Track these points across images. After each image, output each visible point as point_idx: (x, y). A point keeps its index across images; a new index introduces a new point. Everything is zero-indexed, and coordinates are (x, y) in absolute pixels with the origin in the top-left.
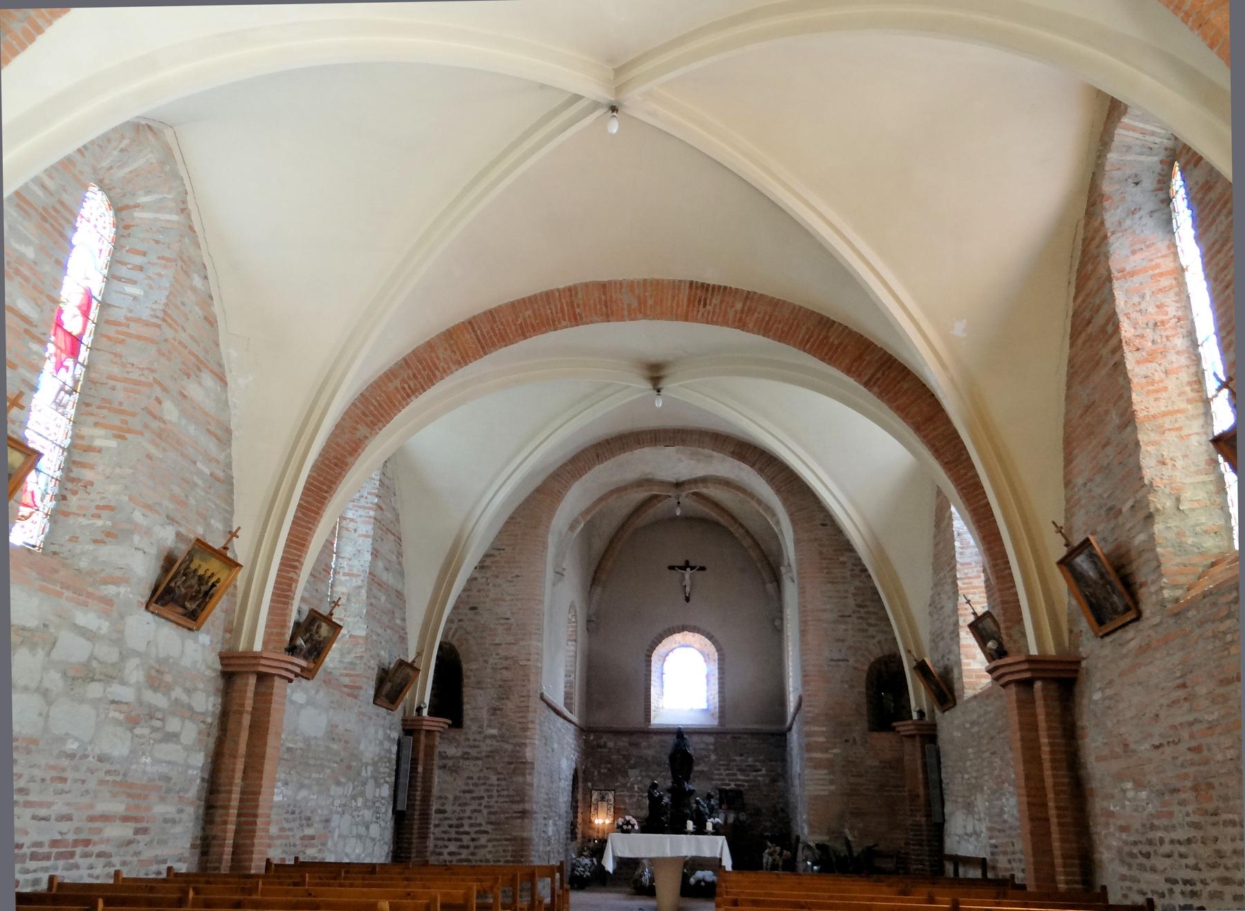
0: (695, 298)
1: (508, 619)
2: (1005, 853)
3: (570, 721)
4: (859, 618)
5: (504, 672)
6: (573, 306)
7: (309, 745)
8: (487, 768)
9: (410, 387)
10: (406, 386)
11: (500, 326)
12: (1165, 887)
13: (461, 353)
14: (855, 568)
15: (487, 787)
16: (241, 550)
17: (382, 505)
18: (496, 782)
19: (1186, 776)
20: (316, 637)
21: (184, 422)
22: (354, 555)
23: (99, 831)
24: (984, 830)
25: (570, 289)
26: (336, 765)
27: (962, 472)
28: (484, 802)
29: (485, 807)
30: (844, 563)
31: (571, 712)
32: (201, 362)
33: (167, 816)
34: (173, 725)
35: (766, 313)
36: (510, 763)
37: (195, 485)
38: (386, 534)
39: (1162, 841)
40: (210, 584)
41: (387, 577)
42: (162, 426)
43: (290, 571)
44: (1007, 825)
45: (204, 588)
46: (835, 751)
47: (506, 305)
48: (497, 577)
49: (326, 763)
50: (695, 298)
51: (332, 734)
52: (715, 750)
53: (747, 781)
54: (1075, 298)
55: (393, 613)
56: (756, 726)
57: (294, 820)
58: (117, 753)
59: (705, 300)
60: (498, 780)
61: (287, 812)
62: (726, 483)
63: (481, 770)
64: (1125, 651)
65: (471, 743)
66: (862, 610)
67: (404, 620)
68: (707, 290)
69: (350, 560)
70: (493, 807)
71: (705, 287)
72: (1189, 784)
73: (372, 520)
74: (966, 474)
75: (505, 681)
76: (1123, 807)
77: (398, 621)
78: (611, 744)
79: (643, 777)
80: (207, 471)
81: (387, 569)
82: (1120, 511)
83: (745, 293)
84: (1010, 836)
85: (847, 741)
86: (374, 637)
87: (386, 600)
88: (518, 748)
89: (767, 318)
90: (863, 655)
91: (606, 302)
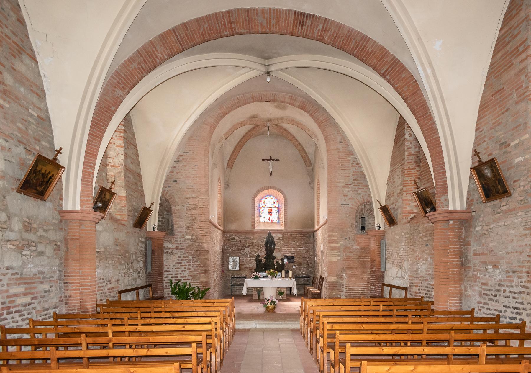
0: (297, 20)
1: (192, 186)
2: (417, 286)
3: (220, 229)
4: (354, 186)
5: (193, 211)
6: (230, 23)
7: (106, 249)
8: (187, 253)
9: (142, 67)
10: (140, 67)
11: (190, 33)
12: (502, 309)
13: (170, 49)
14: (354, 163)
15: (187, 261)
16: (62, 160)
17: (126, 130)
18: (192, 259)
20: (104, 199)
21: (17, 85)
22: (115, 156)
23: (14, 301)
24: (407, 276)
25: (228, 12)
26: (119, 256)
27: (426, 122)
28: (187, 267)
29: (187, 269)
30: (349, 160)
31: (220, 226)
32: (21, 48)
33: (45, 290)
34: (40, 248)
35: (335, 32)
36: (197, 250)
37: (30, 122)
38: (130, 145)
39: (504, 291)
40: (49, 177)
41: (132, 167)
42: (5, 87)
43: (89, 169)
44: (419, 276)
45: (45, 180)
46: (341, 243)
47: (193, 20)
48: (186, 166)
49: (115, 256)
50: (297, 20)
51: (116, 243)
52: (283, 240)
53: (296, 252)
54: (501, 30)
55: (137, 184)
56: (301, 230)
57: (104, 282)
58: (15, 264)
59: (303, 22)
60: (193, 258)
61: (100, 279)
62: (293, 122)
63: (184, 254)
64: (499, 210)
65: (179, 242)
66: (356, 182)
67: (142, 187)
68: (304, 17)
69: (113, 159)
70: (191, 269)
71: (302, 14)
72: (525, 270)
73: (122, 138)
74: (427, 123)
75: (193, 215)
76: (485, 275)
77: (140, 188)
78: (237, 238)
79: (251, 251)
80: (36, 115)
81: (132, 163)
82: (509, 145)
83: (324, 19)
84: (420, 280)
85: (346, 239)
86: (130, 197)
87: (133, 178)
88: (201, 244)
89: (335, 35)
90: (355, 202)
91: (249, 21)
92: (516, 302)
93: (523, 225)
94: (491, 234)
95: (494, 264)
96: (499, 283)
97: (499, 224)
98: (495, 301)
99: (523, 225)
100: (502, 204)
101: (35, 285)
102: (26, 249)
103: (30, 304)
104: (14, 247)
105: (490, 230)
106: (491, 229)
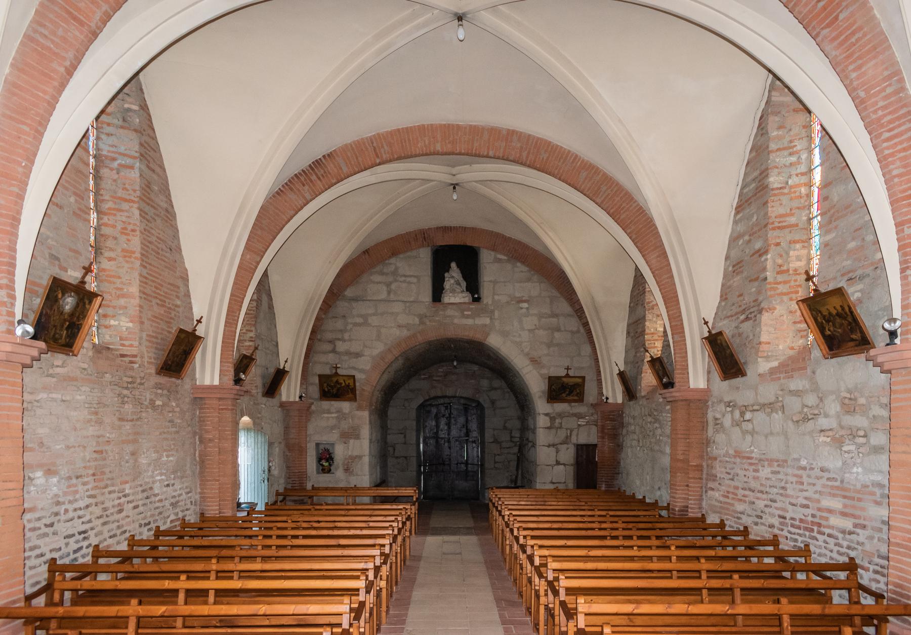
19: (89, 468)
40: (848, 313)
92: (83, 523)
93: (86, 405)
94: (39, 412)
95: (46, 468)
96: (55, 500)
97: (54, 396)
98: (51, 535)
99: (86, 405)
100: (56, 363)
101: (862, 504)
102: (847, 441)
103: (850, 533)
104: (829, 440)
105: (36, 404)
106: (38, 401)
